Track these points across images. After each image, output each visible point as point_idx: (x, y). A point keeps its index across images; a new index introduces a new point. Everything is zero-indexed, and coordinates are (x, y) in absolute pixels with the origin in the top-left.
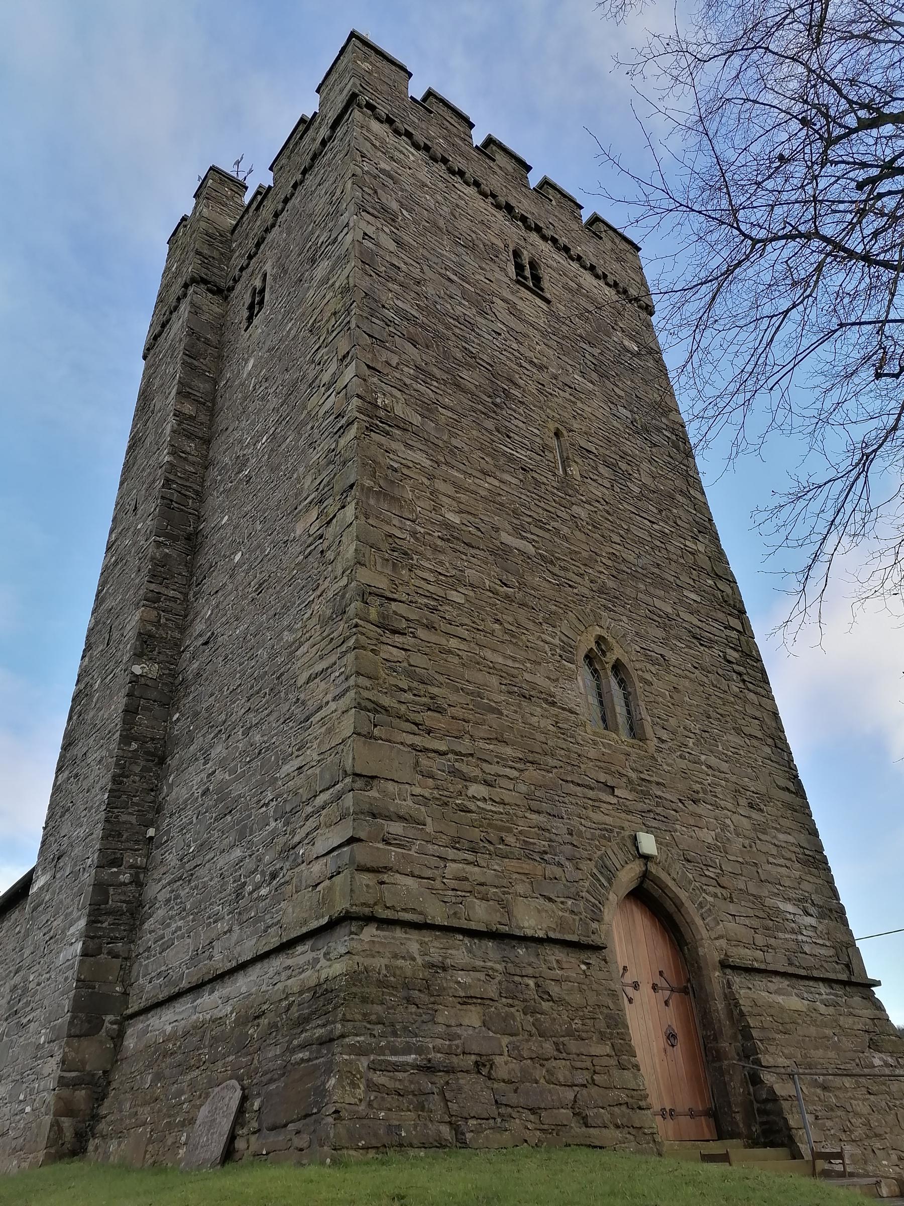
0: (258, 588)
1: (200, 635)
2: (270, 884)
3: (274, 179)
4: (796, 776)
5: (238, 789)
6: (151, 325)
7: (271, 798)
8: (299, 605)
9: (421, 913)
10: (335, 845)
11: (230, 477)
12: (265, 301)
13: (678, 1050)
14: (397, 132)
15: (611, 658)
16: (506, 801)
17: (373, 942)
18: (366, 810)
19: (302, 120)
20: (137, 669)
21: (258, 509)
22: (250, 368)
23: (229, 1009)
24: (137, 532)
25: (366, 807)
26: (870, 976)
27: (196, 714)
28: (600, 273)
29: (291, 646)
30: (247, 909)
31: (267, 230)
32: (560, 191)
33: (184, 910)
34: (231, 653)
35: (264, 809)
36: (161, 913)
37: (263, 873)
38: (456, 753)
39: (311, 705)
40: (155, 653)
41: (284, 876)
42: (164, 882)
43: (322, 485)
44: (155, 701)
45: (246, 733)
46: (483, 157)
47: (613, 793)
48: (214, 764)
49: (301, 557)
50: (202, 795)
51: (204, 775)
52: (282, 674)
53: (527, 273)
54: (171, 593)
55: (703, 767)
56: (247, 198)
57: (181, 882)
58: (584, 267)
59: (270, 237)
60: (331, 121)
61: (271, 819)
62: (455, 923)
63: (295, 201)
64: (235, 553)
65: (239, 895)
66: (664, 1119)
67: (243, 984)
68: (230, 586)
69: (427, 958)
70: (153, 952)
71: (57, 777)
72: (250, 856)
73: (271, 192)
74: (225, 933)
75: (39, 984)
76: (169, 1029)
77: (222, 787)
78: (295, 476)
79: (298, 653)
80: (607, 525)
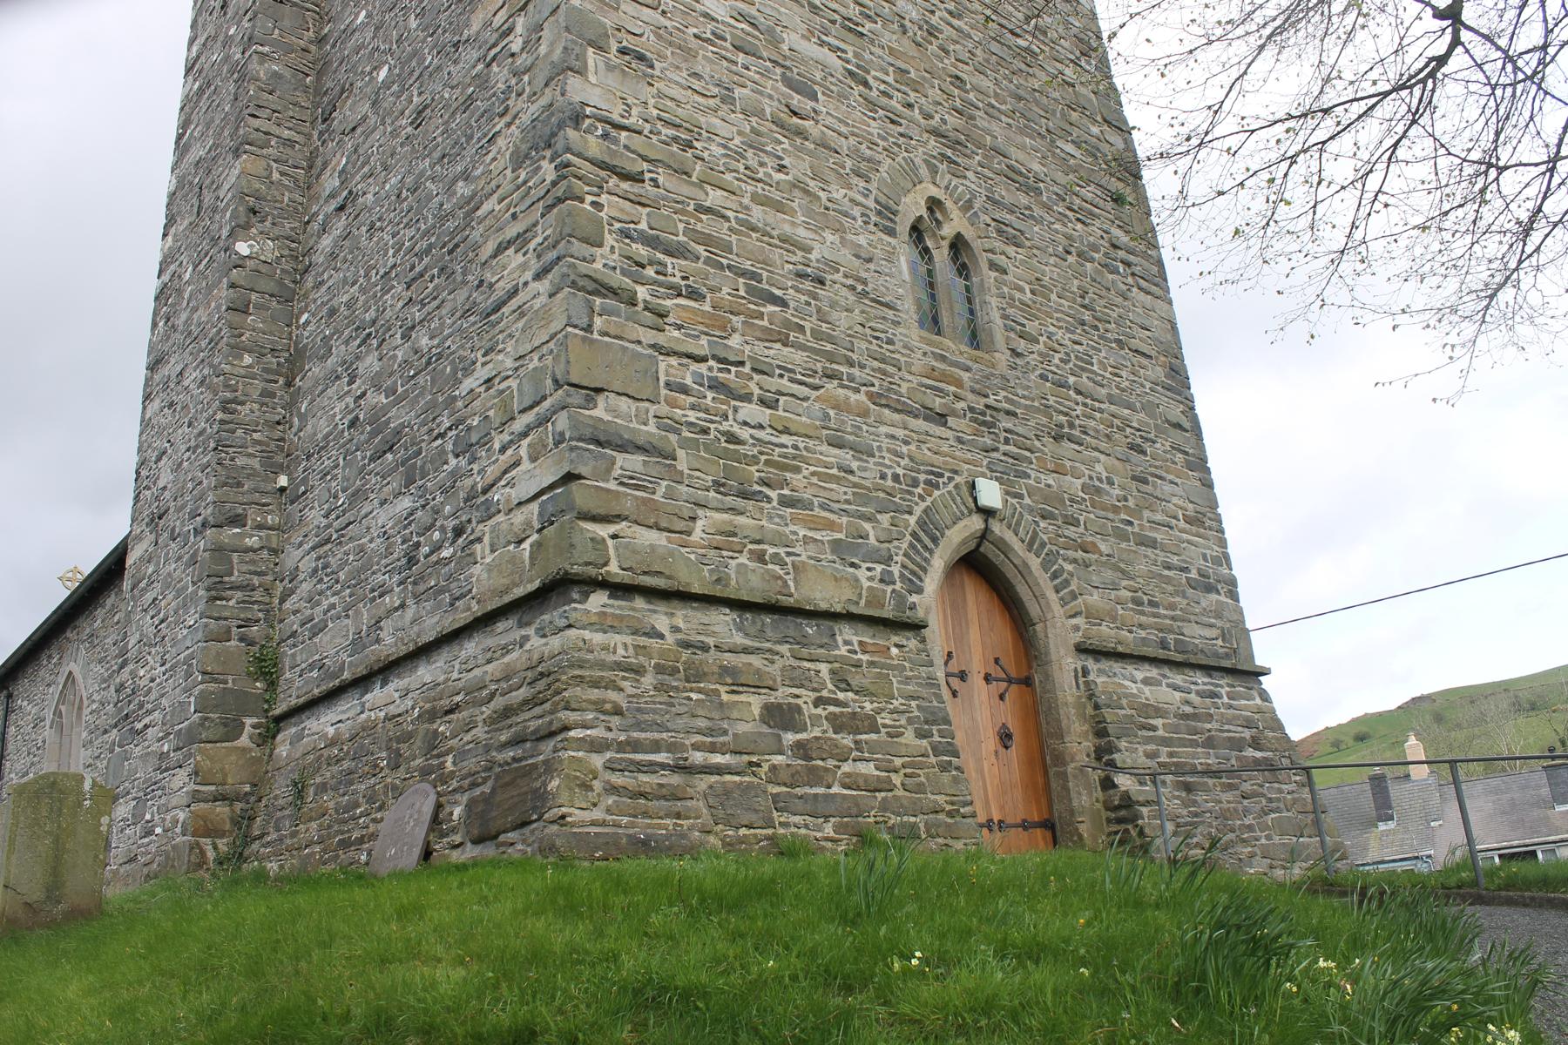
0: (416, 119)
1: (332, 196)
2: (454, 542)
4: (1193, 409)
5: (399, 417)
7: (448, 425)
8: (479, 140)
9: (669, 577)
10: (545, 485)
13: (1014, 752)
15: (948, 231)
16: (793, 430)
17: (604, 613)
23: (410, 703)
24: (228, 42)
25: (588, 432)
26: (1259, 662)
27: (333, 312)
29: (468, 203)
34: (379, 219)
35: (439, 442)
36: (306, 587)
37: (443, 529)
38: (720, 361)
39: (503, 287)
40: (267, 224)
41: (473, 531)
42: (306, 547)
44: (272, 295)
45: (406, 337)
47: (945, 424)
48: (364, 383)
49: (480, 66)
50: (349, 427)
51: (350, 400)
52: (456, 246)
54: (286, 133)
55: (1071, 392)
57: (329, 546)
61: (450, 456)
62: (718, 591)
65: (412, 561)
66: (990, 830)
67: (426, 673)
68: (373, 119)
69: (679, 636)
70: (301, 639)
71: (144, 408)
72: (423, 507)
74: (396, 609)
75: (152, 680)
76: (331, 731)
77: (376, 416)
79: (479, 213)
80: (948, 31)
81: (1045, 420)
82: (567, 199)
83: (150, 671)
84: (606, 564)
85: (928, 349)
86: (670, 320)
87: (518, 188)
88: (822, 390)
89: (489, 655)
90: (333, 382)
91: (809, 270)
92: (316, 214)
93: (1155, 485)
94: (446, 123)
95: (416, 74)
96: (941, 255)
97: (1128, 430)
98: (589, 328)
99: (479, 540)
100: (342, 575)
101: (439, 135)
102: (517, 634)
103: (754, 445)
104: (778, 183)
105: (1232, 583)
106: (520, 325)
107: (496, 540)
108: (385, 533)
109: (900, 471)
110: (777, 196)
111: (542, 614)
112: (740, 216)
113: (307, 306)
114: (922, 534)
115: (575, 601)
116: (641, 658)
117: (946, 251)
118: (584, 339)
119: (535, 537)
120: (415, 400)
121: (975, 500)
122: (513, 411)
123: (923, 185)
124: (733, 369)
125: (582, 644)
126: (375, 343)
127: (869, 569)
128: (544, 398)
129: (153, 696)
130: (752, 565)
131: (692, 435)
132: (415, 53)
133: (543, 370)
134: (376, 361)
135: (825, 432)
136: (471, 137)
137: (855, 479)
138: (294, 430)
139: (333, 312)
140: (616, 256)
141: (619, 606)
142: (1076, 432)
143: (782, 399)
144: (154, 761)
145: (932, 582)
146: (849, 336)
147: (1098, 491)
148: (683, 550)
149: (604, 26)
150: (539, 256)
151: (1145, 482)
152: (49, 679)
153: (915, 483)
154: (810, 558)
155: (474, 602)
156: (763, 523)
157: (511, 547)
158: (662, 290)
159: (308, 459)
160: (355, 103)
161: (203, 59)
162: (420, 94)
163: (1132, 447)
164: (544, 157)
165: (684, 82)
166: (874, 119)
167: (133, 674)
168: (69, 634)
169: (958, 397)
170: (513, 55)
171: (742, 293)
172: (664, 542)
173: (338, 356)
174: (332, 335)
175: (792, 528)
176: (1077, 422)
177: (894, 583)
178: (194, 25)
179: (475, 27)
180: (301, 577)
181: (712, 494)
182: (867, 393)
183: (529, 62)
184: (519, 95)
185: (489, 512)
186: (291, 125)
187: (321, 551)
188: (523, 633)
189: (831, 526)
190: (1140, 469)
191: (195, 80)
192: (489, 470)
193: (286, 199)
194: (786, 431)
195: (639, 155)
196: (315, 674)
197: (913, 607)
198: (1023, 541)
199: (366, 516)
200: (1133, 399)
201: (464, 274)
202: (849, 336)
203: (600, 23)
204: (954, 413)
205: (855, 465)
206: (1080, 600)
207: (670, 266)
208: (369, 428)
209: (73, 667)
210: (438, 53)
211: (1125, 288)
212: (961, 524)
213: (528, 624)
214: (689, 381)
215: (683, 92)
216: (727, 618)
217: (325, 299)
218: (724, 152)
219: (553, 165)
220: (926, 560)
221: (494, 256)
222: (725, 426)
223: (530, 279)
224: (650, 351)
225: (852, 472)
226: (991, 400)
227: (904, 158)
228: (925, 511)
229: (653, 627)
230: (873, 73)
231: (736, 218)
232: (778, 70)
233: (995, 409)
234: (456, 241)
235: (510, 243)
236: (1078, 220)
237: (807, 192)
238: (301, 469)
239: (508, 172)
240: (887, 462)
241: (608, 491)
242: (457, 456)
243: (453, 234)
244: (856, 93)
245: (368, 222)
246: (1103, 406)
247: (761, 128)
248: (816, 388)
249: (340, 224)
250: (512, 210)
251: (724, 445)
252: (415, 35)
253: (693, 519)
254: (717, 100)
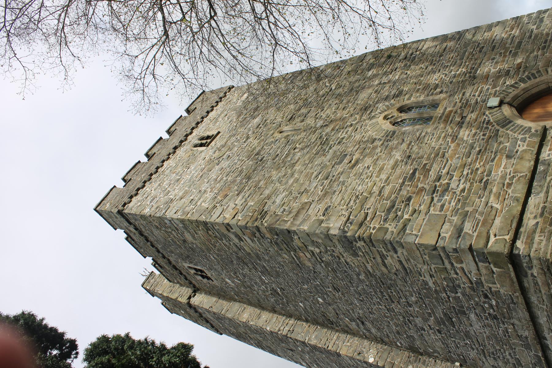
0: (337, 290)
1: (358, 326)
3: (150, 256)
5: (439, 314)
6: (207, 328)
7: (445, 294)
10: (472, 259)
11: (281, 299)
12: (201, 269)
14: (136, 194)
15: (396, 114)
17: (525, 242)
18: (456, 240)
19: (127, 239)
21: (297, 286)
22: (230, 281)
24: (303, 351)
28: (211, 109)
29: (367, 275)
30: (503, 314)
31: (170, 263)
32: (173, 125)
33: (500, 350)
34: (368, 309)
35: (451, 299)
37: (484, 303)
40: (364, 350)
41: (486, 290)
42: (484, 360)
43: (287, 248)
45: (410, 306)
46: (153, 158)
47: (466, 117)
48: (425, 325)
49: (323, 264)
50: (441, 334)
51: (431, 332)
52: (381, 281)
53: (204, 141)
56: (157, 272)
57: (485, 351)
58: (207, 116)
59: (174, 263)
60: (128, 225)
61: (457, 295)
62: (522, 200)
63: (159, 247)
64: (318, 302)
65: (495, 317)
69: (538, 216)
72: (475, 309)
73: (155, 259)
74: (514, 327)
78: (282, 263)
79: (371, 271)
81: (467, 82)
82: (371, 238)
84: (506, 240)
85: (437, 122)
86: (417, 208)
87: (364, 256)
88: (449, 159)
89: (538, 291)
90: (423, 337)
91: (405, 160)
92: (363, 333)
93: (496, 43)
94: (339, 279)
95: (322, 288)
96: (404, 116)
97: (474, 53)
98: (417, 236)
99: (490, 288)
100: (498, 348)
101: (343, 283)
102: (530, 278)
103: (466, 184)
104: (373, 169)
105: (540, 12)
106: (412, 261)
107: (491, 282)
108: (483, 326)
109: (482, 133)
110: (378, 169)
111: (523, 267)
112: (383, 182)
113: (395, 342)
115: (519, 252)
116: (546, 231)
117: (402, 114)
118: (420, 237)
119: (492, 266)
120: (434, 305)
121: (495, 107)
122: (443, 268)
123: (379, 121)
124: (437, 188)
125: (537, 252)
126: (411, 318)
127: (519, 146)
128: (440, 255)
130: (512, 188)
131: (460, 204)
132: (315, 288)
133: (429, 254)
134: (418, 319)
135: (464, 159)
136: (345, 271)
137: (483, 149)
138: (439, 356)
139: (398, 333)
140: (392, 224)
143: (450, 173)
146: (429, 148)
148: (504, 212)
149: (315, 220)
150: (389, 251)
151: (495, 46)
154: (512, 167)
155: (515, 294)
156: (496, 183)
157: (495, 276)
158: (406, 210)
159: (450, 352)
160: (328, 312)
161: (307, 361)
162: (329, 288)
163: (480, 51)
164: (356, 245)
165: (336, 196)
166: (355, 136)
170: (320, 252)
171: (410, 183)
172: (500, 218)
173: (414, 333)
174: (406, 334)
175: (499, 173)
176: (469, 71)
177: (526, 138)
178: (296, 362)
179: (310, 265)
180: (496, 365)
181: (483, 200)
182: (451, 143)
183: (323, 247)
184: (334, 251)
185: (479, 283)
186: (332, 336)
187: (487, 354)
188: (530, 275)
190: (489, 48)
191: (313, 366)
192: (464, 280)
193: (357, 342)
195: (359, 213)
197: (536, 131)
198: (514, 90)
199: (475, 333)
200: (462, 51)
201: (391, 280)
202: (429, 148)
203: (314, 221)
204: (461, 114)
205: (478, 149)
206: (541, 69)
207: (398, 207)
208: (442, 326)
210: (316, 279)
211: (421, 55)
213: (526, 273)
214: (440, 204)
215: (339, 197)
216: (533, 198)
217: (393, 334)
218: (361, 185)
219: (359, 242)
221: (387, 267)
222: (458, 193)
223: (396, 255)
224: (427, 216)
225: (480, 150)
226: (458, 101)
227: (369, 127)
228: (498, 125)
229: (534, 225)
230: (339, 136)
231: (384, 183)
232: (336, 166)
233: (462, 99)
234: (379, 281)
235: (383, 261)
236: (395, 70)
237: (377, 159)
238: (454, 356)
239: (359, 259)
240: (478, 138)
241: (477, 236)
242: (457, 293)
243: (377, 282)
244: (346, 142)
245: (369, 314)
246: (464, 62)
247: (354, 173)
249: (369, 325)
250: (372, 259)
251: (465, 194)
252: (309, 287)
253: (492, 207)
254: (343, 186)
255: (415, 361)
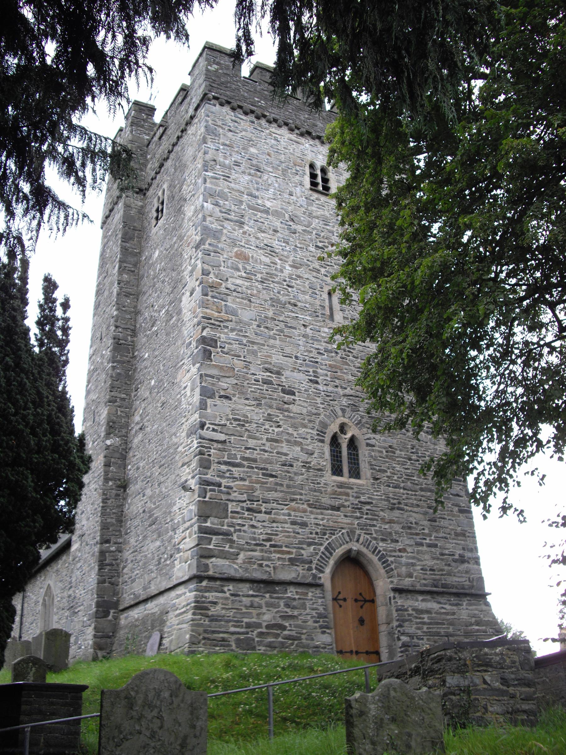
20: (108, 442)
30: (161, 570)
45: (159, 485)
65: (159, 563)
68: (150, 399)
76: (136, 616)
83: (80, 592)
109: (319, 531)
114: (326, 553)
126: (150, 485)
129: (81, 600)
141: (212, 584)
142: (402, 506)
144: (81, 624)
145: (328, 570)
147: (410, 528)
151: (435, 521)
152: (40, 586)
153: (325, 534)
167: (74, 592)
168: (48, 568)
169: (346, 500)
185: (179, 550)
189: (289, 553)
194: (274, 522)
196: (132, 596)
197: (320, 578)
204: (344, 506)
205: (300, 531)
209: (51, 583)
212: (343, 547)
220: (327, 561)
222: (252, 523)
232: (280, 388)
248: (287, 505)
255: (117, 487)
